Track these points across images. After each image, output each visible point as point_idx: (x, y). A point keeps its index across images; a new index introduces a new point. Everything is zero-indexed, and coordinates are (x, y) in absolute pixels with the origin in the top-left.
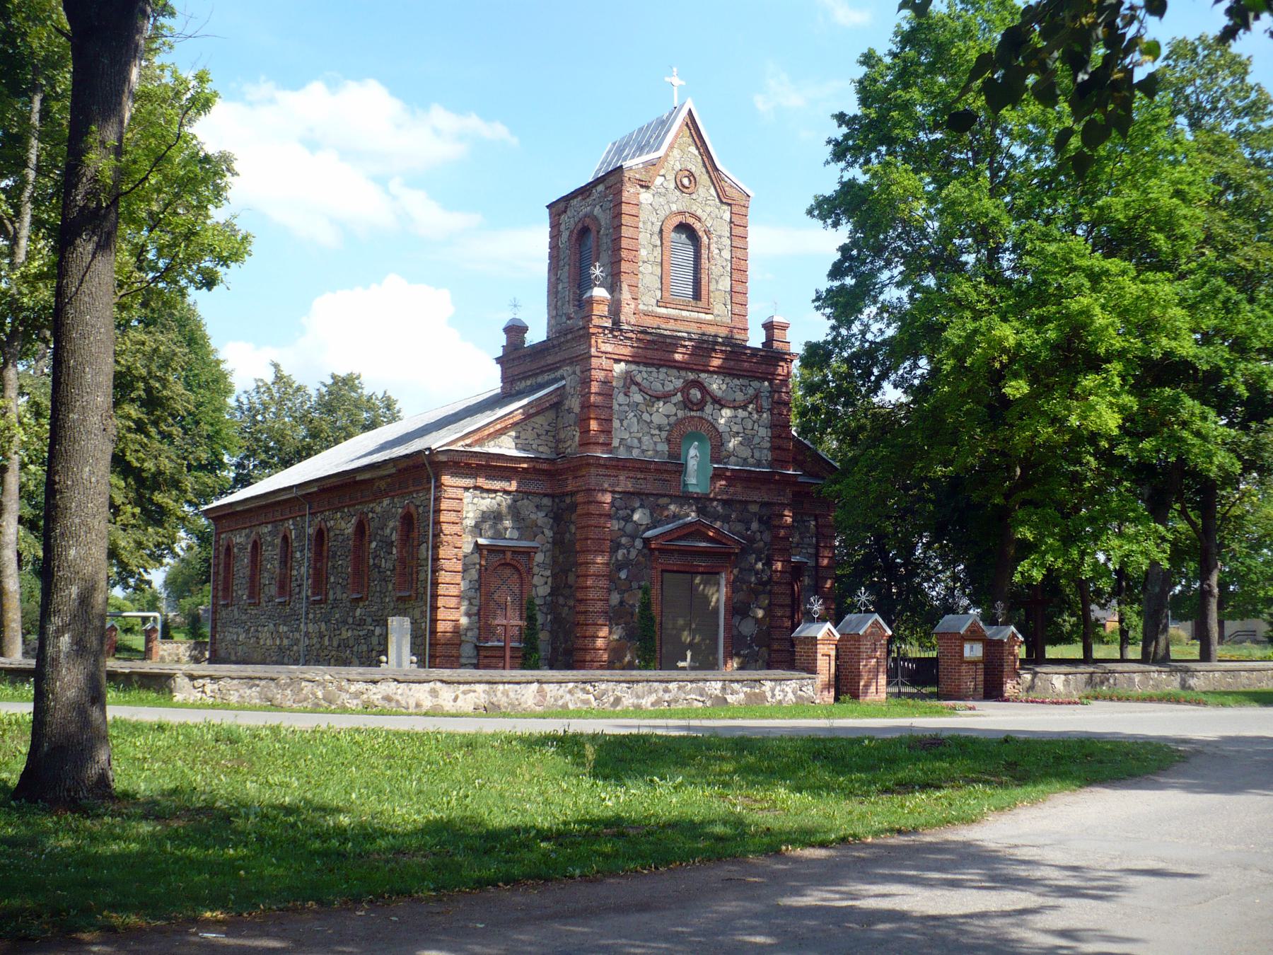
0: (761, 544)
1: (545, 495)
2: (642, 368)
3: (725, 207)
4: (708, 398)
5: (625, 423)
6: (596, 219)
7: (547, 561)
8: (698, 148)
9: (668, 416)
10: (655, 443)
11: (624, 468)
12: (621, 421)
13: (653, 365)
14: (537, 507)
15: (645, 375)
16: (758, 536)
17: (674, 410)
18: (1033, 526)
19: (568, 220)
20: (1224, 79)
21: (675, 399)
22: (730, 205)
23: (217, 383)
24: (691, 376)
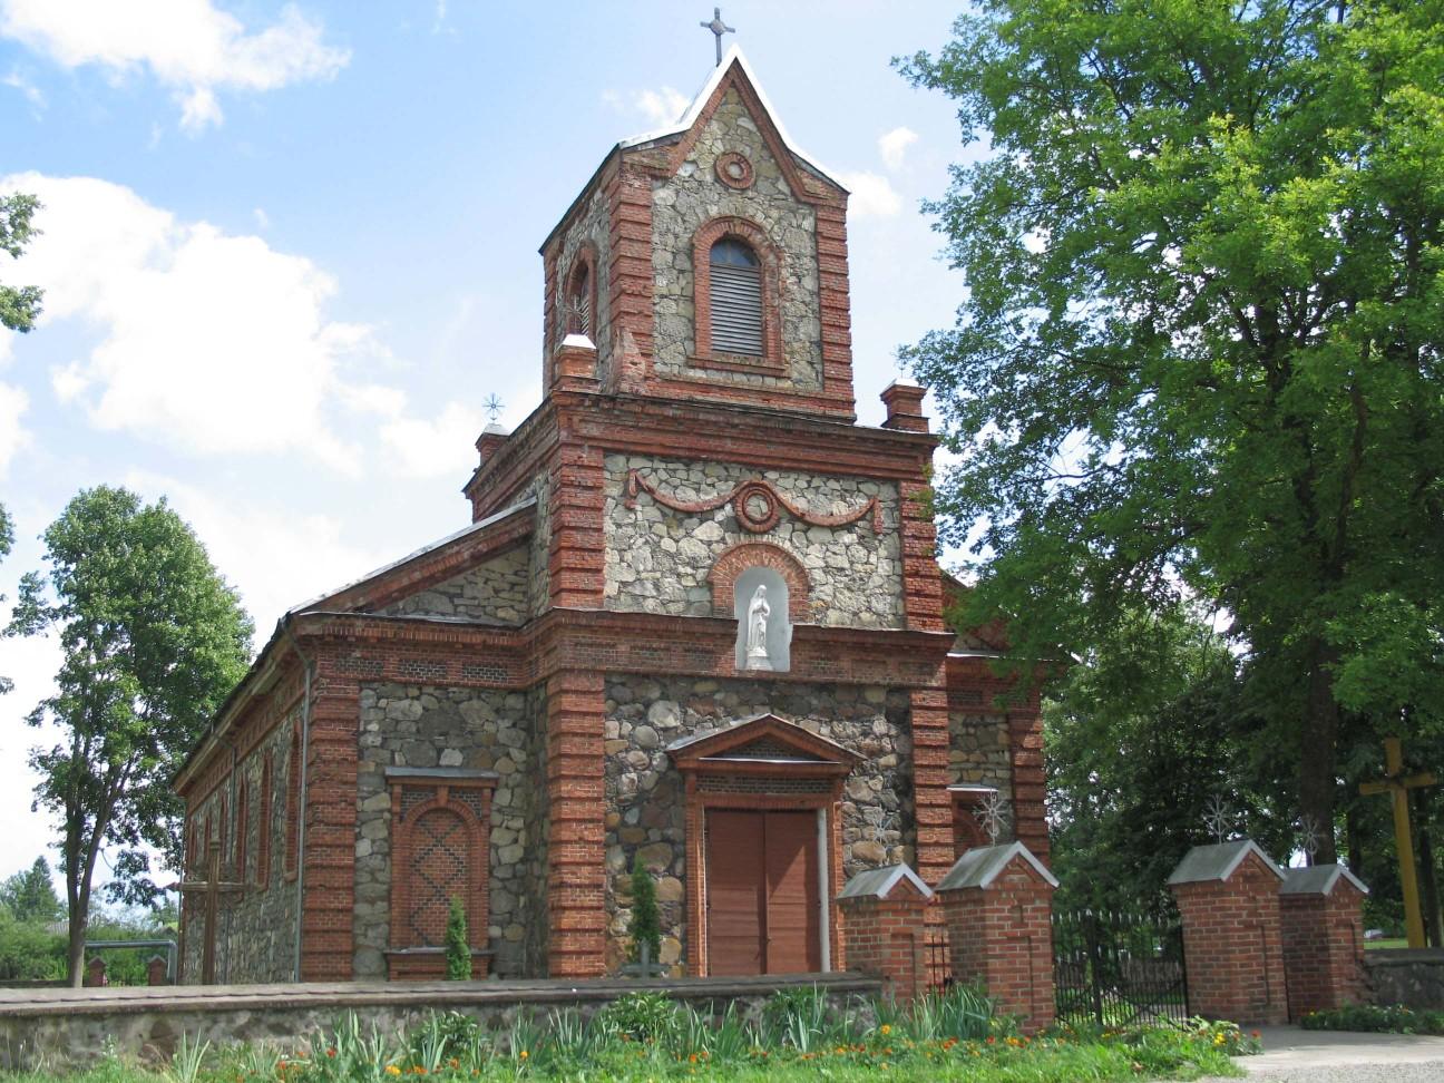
1: (513, 691)
2: (657, 464)
3: (805, 210)
6: (594, 244)
7: (517, 802)
8: (754, 120)
9: (709, 544)
11: (627, 630)
13: (678, 459)
14: (497, 711)
18: (1252, 384)
19: (564, 263)
21: (720, 516)
22: (813, 205)
23: (217, 609)
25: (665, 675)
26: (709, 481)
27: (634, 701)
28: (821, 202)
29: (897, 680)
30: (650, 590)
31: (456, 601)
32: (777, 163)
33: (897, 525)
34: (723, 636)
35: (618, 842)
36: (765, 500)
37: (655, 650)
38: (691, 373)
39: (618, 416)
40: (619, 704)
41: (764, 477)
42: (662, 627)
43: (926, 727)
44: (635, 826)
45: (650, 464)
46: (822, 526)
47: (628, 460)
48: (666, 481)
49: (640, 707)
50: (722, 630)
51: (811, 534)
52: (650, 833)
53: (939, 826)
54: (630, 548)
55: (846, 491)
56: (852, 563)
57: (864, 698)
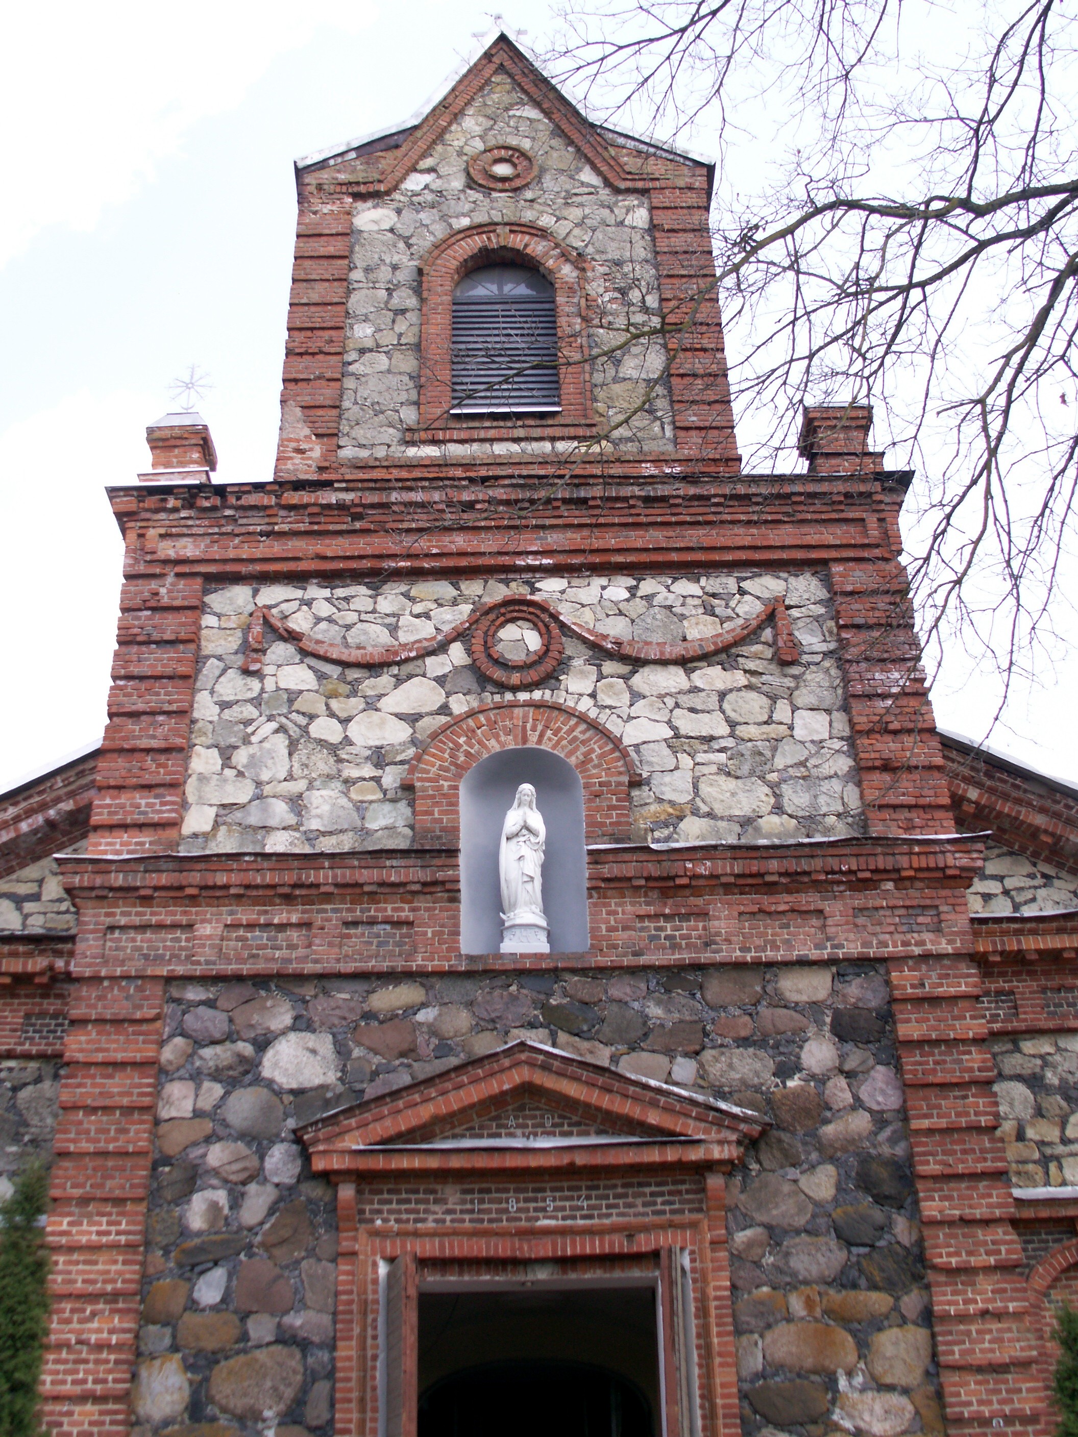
0: (860, 1122)
3: (632, 200)
4: (571, 648)
5: (241, 757)
8: (537, 104)
9: (412, 719)
10: (360, 807)
12: (226, 754)
15: (325, 609)
16: (839, 1091)
17: (437, 697)
20: (745, 1025)
21: (436, 665)
22: (644, 192)
24: (497, 592)
25: (300, 978)
26: (418, 608)
27: (230, 1037)
28: (657, 184)
29: (852, 948)
30: (280, 811)
31: (29, 907)
32: (578, 150)
33: (832, 646)
34: (428, 887)
35: (175, 1348)
36: (536, 627)
37: (282, 927)
38: (412, 452)
39: (233, 519)
40: (199, 1044)
41: (534, 590)
42: (289, 877)
43: (937, 1042)
44: (214, 1308)
45: (299, 593)
46: (663, 663)
47: (256, 593)
48: (330, 620)
49: (246, 1049)
50: (424, 875)
51: (637, 680)
52: (251, 1324)
53: (988, 1270)
54: (246, 741)
55: (714, 595)
56: (732, 724)
57: (778, 993)
